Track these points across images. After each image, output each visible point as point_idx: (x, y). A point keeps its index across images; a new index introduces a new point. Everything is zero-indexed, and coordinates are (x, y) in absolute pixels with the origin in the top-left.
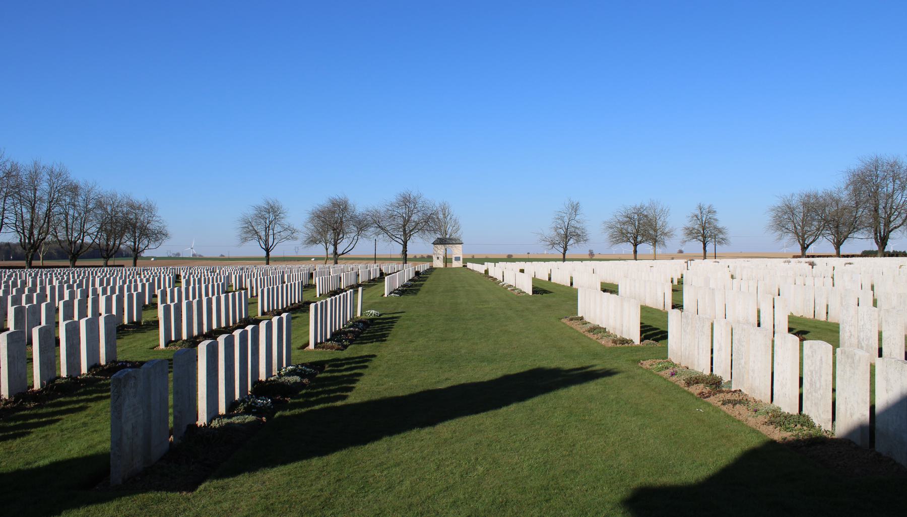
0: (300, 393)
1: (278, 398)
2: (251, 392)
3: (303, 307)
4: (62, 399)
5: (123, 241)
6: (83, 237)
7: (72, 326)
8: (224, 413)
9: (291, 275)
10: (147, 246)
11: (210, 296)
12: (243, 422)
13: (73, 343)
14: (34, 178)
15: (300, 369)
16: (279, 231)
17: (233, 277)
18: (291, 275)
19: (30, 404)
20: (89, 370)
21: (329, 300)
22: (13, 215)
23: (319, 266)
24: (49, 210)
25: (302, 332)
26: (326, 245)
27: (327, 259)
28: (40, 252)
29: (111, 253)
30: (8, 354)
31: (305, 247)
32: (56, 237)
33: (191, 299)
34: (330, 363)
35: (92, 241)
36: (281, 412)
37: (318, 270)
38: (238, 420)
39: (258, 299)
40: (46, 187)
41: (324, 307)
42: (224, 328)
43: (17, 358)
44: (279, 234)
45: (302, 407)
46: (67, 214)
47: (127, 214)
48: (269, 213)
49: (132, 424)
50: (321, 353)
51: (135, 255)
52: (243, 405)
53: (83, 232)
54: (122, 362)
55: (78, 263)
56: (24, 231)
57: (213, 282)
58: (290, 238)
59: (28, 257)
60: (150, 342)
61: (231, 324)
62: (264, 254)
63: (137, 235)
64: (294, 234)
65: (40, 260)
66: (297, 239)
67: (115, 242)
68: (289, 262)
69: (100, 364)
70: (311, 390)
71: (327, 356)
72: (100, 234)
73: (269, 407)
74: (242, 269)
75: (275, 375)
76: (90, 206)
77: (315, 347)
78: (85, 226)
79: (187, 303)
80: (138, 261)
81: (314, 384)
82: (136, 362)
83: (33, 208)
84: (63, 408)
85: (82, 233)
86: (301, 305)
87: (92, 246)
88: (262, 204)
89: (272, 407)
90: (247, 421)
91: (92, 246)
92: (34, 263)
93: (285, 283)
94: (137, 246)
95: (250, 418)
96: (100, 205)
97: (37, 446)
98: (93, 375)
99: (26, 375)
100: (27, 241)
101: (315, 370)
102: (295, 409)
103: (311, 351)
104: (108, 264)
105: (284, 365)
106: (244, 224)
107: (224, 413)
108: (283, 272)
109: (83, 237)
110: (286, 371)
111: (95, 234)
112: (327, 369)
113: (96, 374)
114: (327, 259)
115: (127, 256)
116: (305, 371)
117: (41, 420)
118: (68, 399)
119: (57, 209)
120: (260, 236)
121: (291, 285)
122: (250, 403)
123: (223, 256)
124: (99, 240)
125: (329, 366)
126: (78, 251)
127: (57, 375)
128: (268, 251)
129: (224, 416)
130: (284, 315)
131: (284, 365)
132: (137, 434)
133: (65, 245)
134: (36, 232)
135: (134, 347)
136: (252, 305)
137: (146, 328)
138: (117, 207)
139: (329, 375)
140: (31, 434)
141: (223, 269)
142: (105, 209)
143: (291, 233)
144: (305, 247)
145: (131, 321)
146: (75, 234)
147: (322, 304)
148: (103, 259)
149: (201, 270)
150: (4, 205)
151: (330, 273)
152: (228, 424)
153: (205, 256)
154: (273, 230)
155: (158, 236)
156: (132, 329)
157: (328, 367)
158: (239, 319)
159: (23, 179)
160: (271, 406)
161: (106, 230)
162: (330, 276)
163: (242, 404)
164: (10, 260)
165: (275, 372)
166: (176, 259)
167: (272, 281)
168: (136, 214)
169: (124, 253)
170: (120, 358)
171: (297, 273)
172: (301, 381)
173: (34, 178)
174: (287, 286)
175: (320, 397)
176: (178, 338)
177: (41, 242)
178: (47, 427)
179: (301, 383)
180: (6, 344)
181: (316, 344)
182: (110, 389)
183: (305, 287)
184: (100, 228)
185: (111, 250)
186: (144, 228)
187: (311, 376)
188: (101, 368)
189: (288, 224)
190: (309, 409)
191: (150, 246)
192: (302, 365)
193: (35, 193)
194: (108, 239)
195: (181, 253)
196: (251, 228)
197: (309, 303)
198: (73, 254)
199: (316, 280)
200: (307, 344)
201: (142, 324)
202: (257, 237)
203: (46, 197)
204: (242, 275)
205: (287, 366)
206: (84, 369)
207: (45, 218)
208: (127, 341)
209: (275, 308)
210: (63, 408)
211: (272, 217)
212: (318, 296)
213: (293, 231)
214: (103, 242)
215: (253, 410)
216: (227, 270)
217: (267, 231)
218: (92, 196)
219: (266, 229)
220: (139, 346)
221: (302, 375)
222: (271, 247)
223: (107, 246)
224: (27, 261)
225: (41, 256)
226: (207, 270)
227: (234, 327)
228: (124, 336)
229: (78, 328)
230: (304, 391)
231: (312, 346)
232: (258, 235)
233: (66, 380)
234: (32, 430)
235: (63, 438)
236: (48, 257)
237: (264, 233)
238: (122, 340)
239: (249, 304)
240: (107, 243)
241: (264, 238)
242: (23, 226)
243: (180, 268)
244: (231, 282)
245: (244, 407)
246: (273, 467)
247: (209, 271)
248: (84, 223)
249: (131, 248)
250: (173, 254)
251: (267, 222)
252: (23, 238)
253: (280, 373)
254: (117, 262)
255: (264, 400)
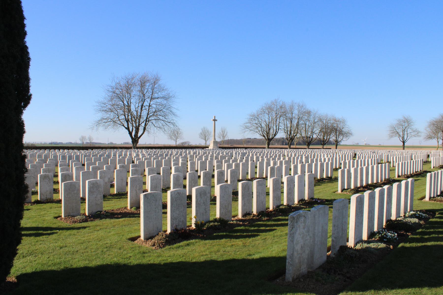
0: (418, 231)
1: (402, 232)
2: (385, 226)
3: (423, 174)
4: (280, 217)
5: (331, 137)
6: (313, 135)
7: (290, 178)
8: (366, 239)
9: (416, 155)
10: (342, 139)
11: (373, 165)
12: (377, 247)
13: (290, 187)
14: (292, 108)
15: (419, 214)
16: (410, 132)
17: (384, 155)
18: (416, 155)
19: (265, 218)
20: (299, 202)
21: (440, 171)
22: (283, 125)
23: (433, 151)
24: (298, 122)
25: (422, 189)
26: (438, 139)
27: (438, 147)
28: (295, 141)
29: (325, 142)
30: (256, 191)
31: (426, 141)
32: (301, 135)
33: (373, 165)
34: (439, 212)
35: (316, 137)
36: (403, 243)
37: (432, 153)
38: (374, 245)
39: (395, 168)
40: (296, 112)
41: (436, 176)
42: (375, 183)
43: (261, 193)
44: (410, 134)
45: (419, 242)
46: (306, 124)
47: (333, 124)
48: (405, 123)
49: (301, 245)
50: (433, 204)
51: (337, 143)
52: (379, 235)
53: (312, 132)
54: (316, 199)
55: (310, 147)
56: (287, 132)
57: (375, 158)
58: (417, 136)
59: (289, 144)
60: (334, 188)
61: (379, 181)
62: (402, 144)
63: (338, 134)
64: (419, 134)
65: (294, 145)
66: (420, 136)
67: (327, 137)
68: (416, 149)
69: (305, 199)
70: (425, 230)
71: (437, 206)
72: (320, 133)
73: (396, 239)
74: (390, 151)
75: (402, 217)
76: (316, 121)
77: (429, 200)
78: (314, 130)
79: (371, 166)
80: (337, 146)
81: (428, 225)
82: (324, 199)
83: (291, 122)
84: (279, 223)
85: (312, 133)
86: (422, 173)
87: (317, 139)
88: (401, 118)
89: (397, 239)
90: (379, 247)
91: (317, 139)
92: (292, 146)
93: (412, 159)
94: (337, 139)
95: (382, 245)
96: (321, 120)
97: (259, 244)
98: (300, 205)
99: (265, 202)
100: (289, 137)
101: (429, 215)
102: (413, 243)
103: (426, 202)
104: (324, 148)
105: (408, 210)
106: (391, 129)
107: (366, 239)
108: (412, 154)
109: (313, 135)
110: (409, 214)
111: (318, 133)
112: (437, 216)
113: (302, 205)
114: (438, 148)
115: (334, 144)
116: (422, 215)
117: (267, 228)
118: (283, 218)
119: (301, 122)
120: (400, 135)
121: (416, 161)
122: (383, 235)
123: (369, 145)
124: (320, 136)
125: (439, 214)
126: (311, 141)
127: (281, 204)
128: (404, 142)
129: (365, 242)
130: (410, 180)
131: (408, 210)
132: (304, 251)
133: (305, 139)
134: (292, 132)
135: (325, 191)
136: (393, 171)
137: (334, 180)
138: (328, 120)
139: (438, 220)
140: (258, 236)
141: (379, 151)
142: (323, 122)
143: (417, 133)
144: (426, 141)
145: (327, 176)
146: (309, 134)
147: (435, 174)
148: (321, 145)
149: (368, 151)
150: (279, 121)
151: (440, 155)
152: (367, 248)
153: (371, 144)
154: (407, 132)
155: (348, 134)
156: (327, 181)
157: (438, 214)
158: (384, 179)
159: (287, 108)
160: (397, 238)
161: (323, 132)
162: (440, 157)
163: (378, 234)
164: (283, 145)
165: (402, 214)
166: (357, 146)
167: (405, 158)
168: (337, 124)
169: (332, 143)
170: (316, 197)
171: (420, 155)
172: (419, 222)
173: (292, 108)
174: (413, 161)
175: (431, 236)
176: (348, 188)
177: (294, 137)
178: (267, 234)
179: (419, 223)
180: (256, 186)
181: (430, 198)
182: (288, 224)
183: (425, 162)
184: (320, 131)
185: (325, 141)
186: (341, 131)
187: (426, 219)
188: (304, 201)
189: (415, 129)
190: (423, 244)
191: (344, 139)
192: (421, 211)
193: (292, 115)
194: (324, 136)
195: (359, 143)
196: (395, 131)
197: (427, 172)
198: (308, 142)
199: (431, 159)
200: (424, 197)
201: (333, 178)
202: (398, 135)
203: (297, 117)
204: (388, 155)
205: (410, 211)
206: (296, 202)
207: (296, 126)
208: (323, 187)
209: (406, 174)
210: (279, 223)
211: (406, 125)
212: (432, 168)
213: (418, 132)
214: (322, 137)
215: (385, 240)
216: (381, 152)
217: (404, 132)
218: (317, 115)
219: (403, 131)
220: (328, 190)
221: (420, 218)
222: (405, 140)
223: (323, 139)
224: (289, 146)
225: (295, 143)
226: (370, 152)
227: (381, 183)
228: (322, 184)
229: (293, 179)
230: (420, 230)
231: (427, 199)
232: (398, 134)
233: (285, 207)
234: (260, 234)
235: (273, 241)
236: (299, 144)
237: (402, 133)
238: (320, 186)
239: (391, 170)
240: (323, 138)
241: (402, 136)
242: (287, 130)
243: (357, 150)
244: (383, 158)
245: (379, 237)
246: (392, 289)
247: (371, 152)
248: (313, 128)
249: (334, 140)
250: (355, 143)
251: (404, 127)
252: (287, 135)
253: (405, 215)
254: (328, 147)
255: (392, 233)
